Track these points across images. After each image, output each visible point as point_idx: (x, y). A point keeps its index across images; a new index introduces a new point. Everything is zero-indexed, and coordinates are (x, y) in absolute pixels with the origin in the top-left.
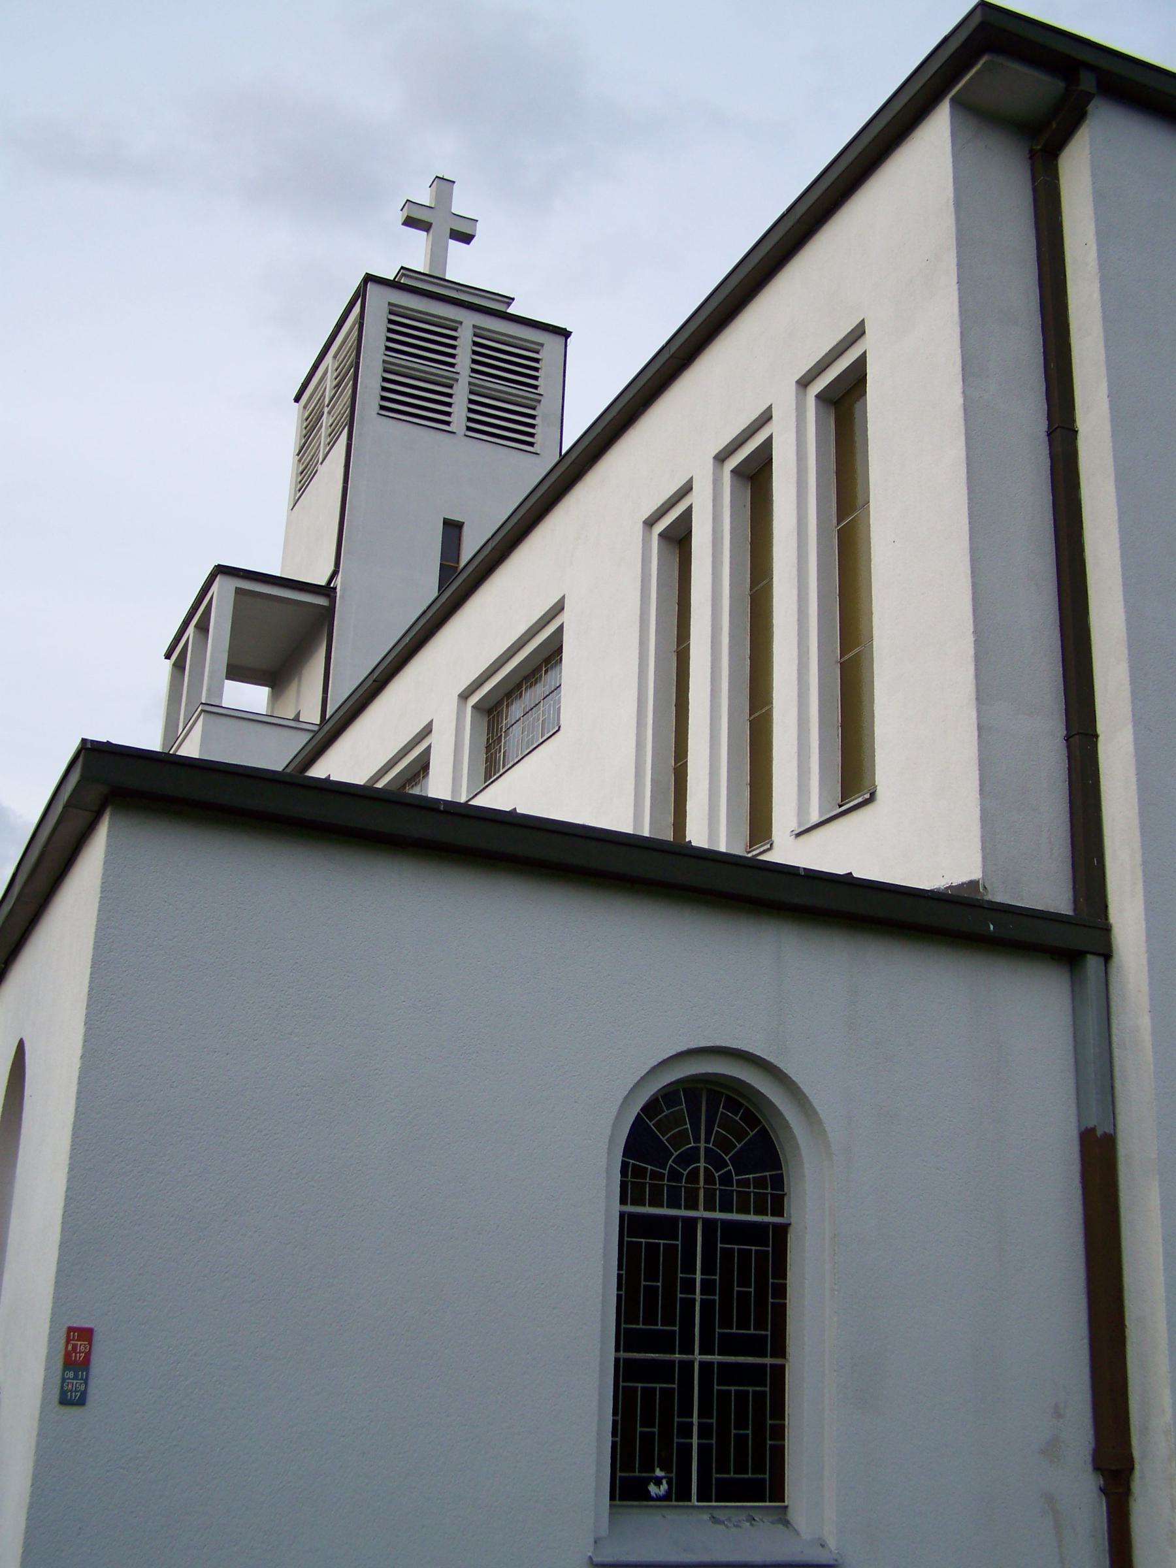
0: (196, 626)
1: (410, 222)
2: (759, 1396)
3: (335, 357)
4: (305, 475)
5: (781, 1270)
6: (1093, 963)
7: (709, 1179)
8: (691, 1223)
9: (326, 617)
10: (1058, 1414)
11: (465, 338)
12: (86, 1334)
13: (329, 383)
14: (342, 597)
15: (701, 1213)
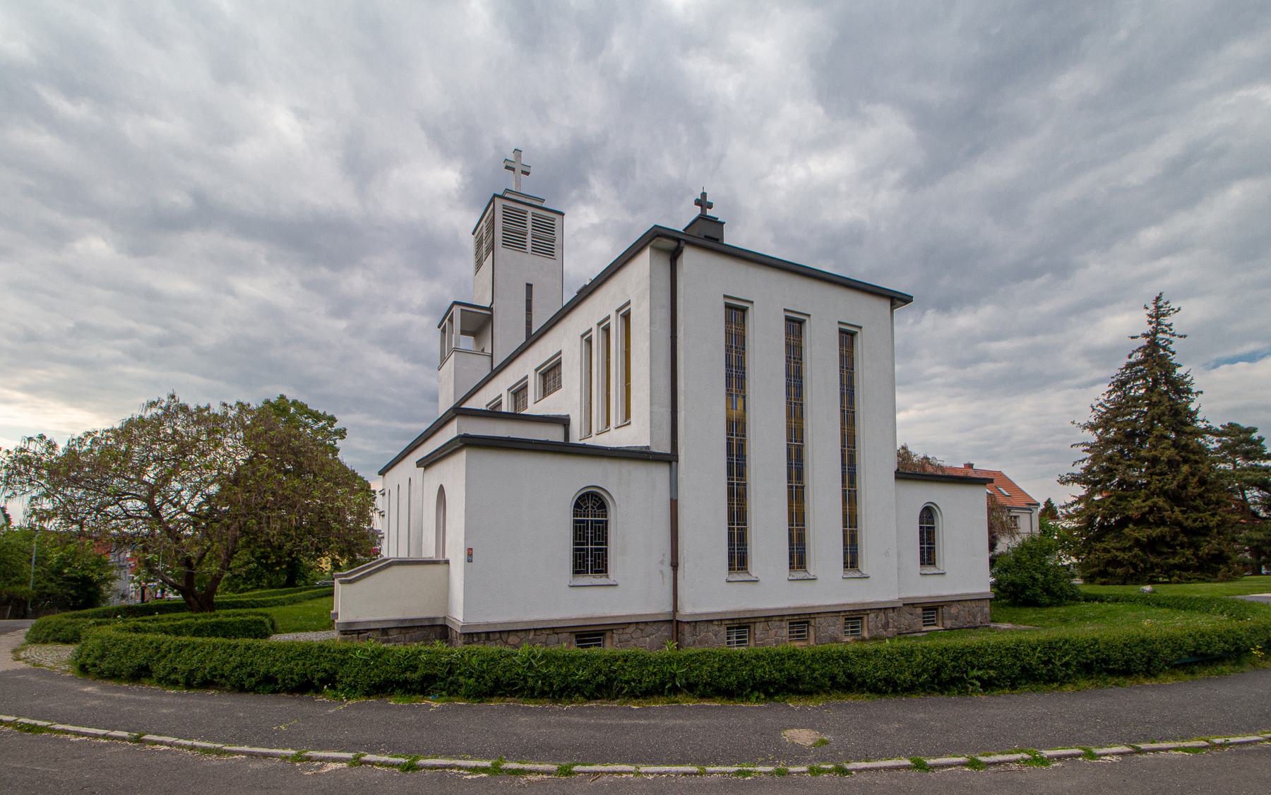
1: (507, 167)
2: (602, 554)
4: (479, 264)
5: (606, 529)
6: (674, 463)
7: (591, 511)
8: (588, 521)
9: (490, 318)
10: (664, 555)
11: (529, 217)
12: (471, 549)
13: (484, 229)
15: (590, 518)
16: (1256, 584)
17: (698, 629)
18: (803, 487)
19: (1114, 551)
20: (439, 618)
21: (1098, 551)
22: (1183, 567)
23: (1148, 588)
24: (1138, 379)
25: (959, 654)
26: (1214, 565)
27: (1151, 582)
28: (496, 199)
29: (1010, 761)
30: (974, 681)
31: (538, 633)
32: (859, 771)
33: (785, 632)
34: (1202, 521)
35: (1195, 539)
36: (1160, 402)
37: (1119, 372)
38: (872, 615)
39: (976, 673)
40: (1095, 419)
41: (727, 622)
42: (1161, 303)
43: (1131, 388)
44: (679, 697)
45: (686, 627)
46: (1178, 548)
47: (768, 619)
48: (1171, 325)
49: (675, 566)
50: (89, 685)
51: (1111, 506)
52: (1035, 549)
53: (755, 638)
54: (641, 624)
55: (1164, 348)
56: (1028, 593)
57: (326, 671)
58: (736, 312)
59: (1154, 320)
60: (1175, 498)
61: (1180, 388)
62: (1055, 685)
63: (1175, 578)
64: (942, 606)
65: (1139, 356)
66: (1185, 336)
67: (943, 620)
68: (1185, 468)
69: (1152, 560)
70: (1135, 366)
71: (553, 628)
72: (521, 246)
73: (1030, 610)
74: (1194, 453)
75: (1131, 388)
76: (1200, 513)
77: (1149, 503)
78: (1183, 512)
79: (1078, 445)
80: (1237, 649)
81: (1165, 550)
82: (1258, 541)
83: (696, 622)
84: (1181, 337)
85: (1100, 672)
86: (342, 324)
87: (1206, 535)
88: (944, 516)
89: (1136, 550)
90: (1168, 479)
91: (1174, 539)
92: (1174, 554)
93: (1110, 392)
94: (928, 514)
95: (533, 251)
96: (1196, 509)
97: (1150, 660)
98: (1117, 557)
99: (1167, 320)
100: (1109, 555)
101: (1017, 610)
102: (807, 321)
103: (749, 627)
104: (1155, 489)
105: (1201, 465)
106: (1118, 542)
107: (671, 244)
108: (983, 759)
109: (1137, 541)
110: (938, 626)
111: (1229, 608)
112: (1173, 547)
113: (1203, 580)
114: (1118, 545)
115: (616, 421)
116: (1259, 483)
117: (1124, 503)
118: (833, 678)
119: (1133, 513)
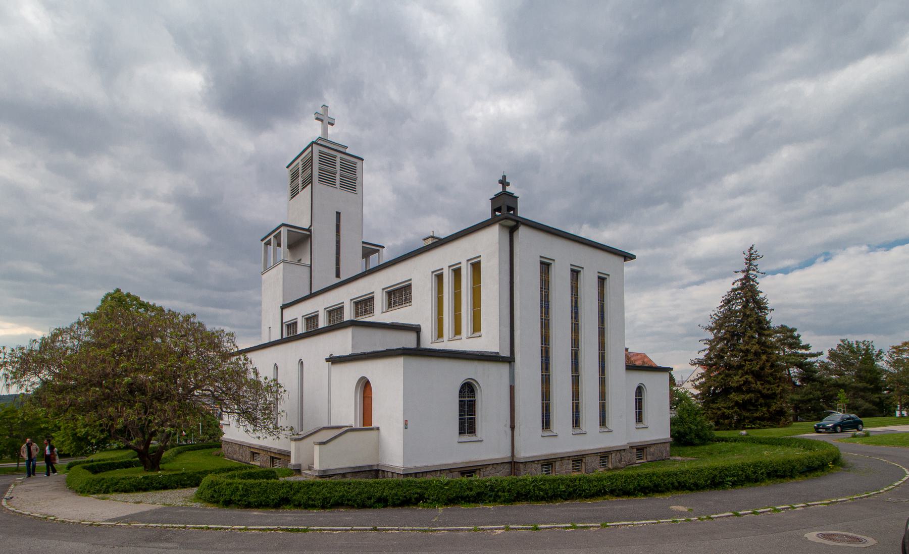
0: (274, 236)
1: (317, 119)
3: (302, 160)
6: (512, 363)
9: (310, 236)
11: (338, 160)
12: (407, 421)
14: (313, 233)
15: (466, 399)
16: (800, 428)
17: (527, 467)
18: (578, 376)
20: (374, 465)
22: (762, 419)
23: (744, 432)
25: (722, 470)
26: (778, 417)
27: (744, 428)
28: (314, 145)
29: (767, 511)
30: (728, 483)
31: (442, 472)
32: (716, 518)
33: (570, 466)
34: (772, 390)
35: (768, 401)
36: (751, 315)
37: (727, 294)
38: (614, 455)
39: (729, 479)
41: (542, 462)
42: (752, 251)
43: (733, 304)
44: (607, 497)
45: (521, 465)
46: (759, 406)
47: (562, 458)
48: (757, 265)
49: (513, 427)
50: (256, 512)
51: (722, 381)
52: (691, 410)
54: (495, 465)
56: (687, 438)
57: (418, 493)
58: (545, 266)
60: (758, 376)
61: (760, 306)
62: (758, 483)
66: (765, 273)
67: (646, 456)
68: (764, 357)
69: (744, 414)
71: (450, 469)
73: (689, 448)
74: (768, 347)
75: (733, 304)
76: (771, 384)
77: (743, 378)
78: (762, 384)
79: (703, 340)
81: (751, 408)
82: (797, 400)
83: (526, 462)
84: (762, 274)
85: (773, 477)
86: (87, 207)
87: (773, 398)
88: (647, 389)
89: (736, 408)
90: (754, 364)
91: (756, 401)
92: (757, 410)
93: (721, 307)
94: (640, 390)
95: (341, 187)
96: (769, 383)
97: (792, 470)
98: (724, 413)
99: (755, 262)
100: (720, 412)
101: (681, 448)
102: (582, 272)
103: (552, 464)
104: (747, 370)
105: (772, 355)
107: (512, 223)
108: (740, 513)
109: (737, 403)
111: (802, 444)
112: (756, 406)
113: (772, 427)
114: (725, 405)
115: (467, 334)
116: (798, 364)
117: (729, 379)
118: (672, 484)
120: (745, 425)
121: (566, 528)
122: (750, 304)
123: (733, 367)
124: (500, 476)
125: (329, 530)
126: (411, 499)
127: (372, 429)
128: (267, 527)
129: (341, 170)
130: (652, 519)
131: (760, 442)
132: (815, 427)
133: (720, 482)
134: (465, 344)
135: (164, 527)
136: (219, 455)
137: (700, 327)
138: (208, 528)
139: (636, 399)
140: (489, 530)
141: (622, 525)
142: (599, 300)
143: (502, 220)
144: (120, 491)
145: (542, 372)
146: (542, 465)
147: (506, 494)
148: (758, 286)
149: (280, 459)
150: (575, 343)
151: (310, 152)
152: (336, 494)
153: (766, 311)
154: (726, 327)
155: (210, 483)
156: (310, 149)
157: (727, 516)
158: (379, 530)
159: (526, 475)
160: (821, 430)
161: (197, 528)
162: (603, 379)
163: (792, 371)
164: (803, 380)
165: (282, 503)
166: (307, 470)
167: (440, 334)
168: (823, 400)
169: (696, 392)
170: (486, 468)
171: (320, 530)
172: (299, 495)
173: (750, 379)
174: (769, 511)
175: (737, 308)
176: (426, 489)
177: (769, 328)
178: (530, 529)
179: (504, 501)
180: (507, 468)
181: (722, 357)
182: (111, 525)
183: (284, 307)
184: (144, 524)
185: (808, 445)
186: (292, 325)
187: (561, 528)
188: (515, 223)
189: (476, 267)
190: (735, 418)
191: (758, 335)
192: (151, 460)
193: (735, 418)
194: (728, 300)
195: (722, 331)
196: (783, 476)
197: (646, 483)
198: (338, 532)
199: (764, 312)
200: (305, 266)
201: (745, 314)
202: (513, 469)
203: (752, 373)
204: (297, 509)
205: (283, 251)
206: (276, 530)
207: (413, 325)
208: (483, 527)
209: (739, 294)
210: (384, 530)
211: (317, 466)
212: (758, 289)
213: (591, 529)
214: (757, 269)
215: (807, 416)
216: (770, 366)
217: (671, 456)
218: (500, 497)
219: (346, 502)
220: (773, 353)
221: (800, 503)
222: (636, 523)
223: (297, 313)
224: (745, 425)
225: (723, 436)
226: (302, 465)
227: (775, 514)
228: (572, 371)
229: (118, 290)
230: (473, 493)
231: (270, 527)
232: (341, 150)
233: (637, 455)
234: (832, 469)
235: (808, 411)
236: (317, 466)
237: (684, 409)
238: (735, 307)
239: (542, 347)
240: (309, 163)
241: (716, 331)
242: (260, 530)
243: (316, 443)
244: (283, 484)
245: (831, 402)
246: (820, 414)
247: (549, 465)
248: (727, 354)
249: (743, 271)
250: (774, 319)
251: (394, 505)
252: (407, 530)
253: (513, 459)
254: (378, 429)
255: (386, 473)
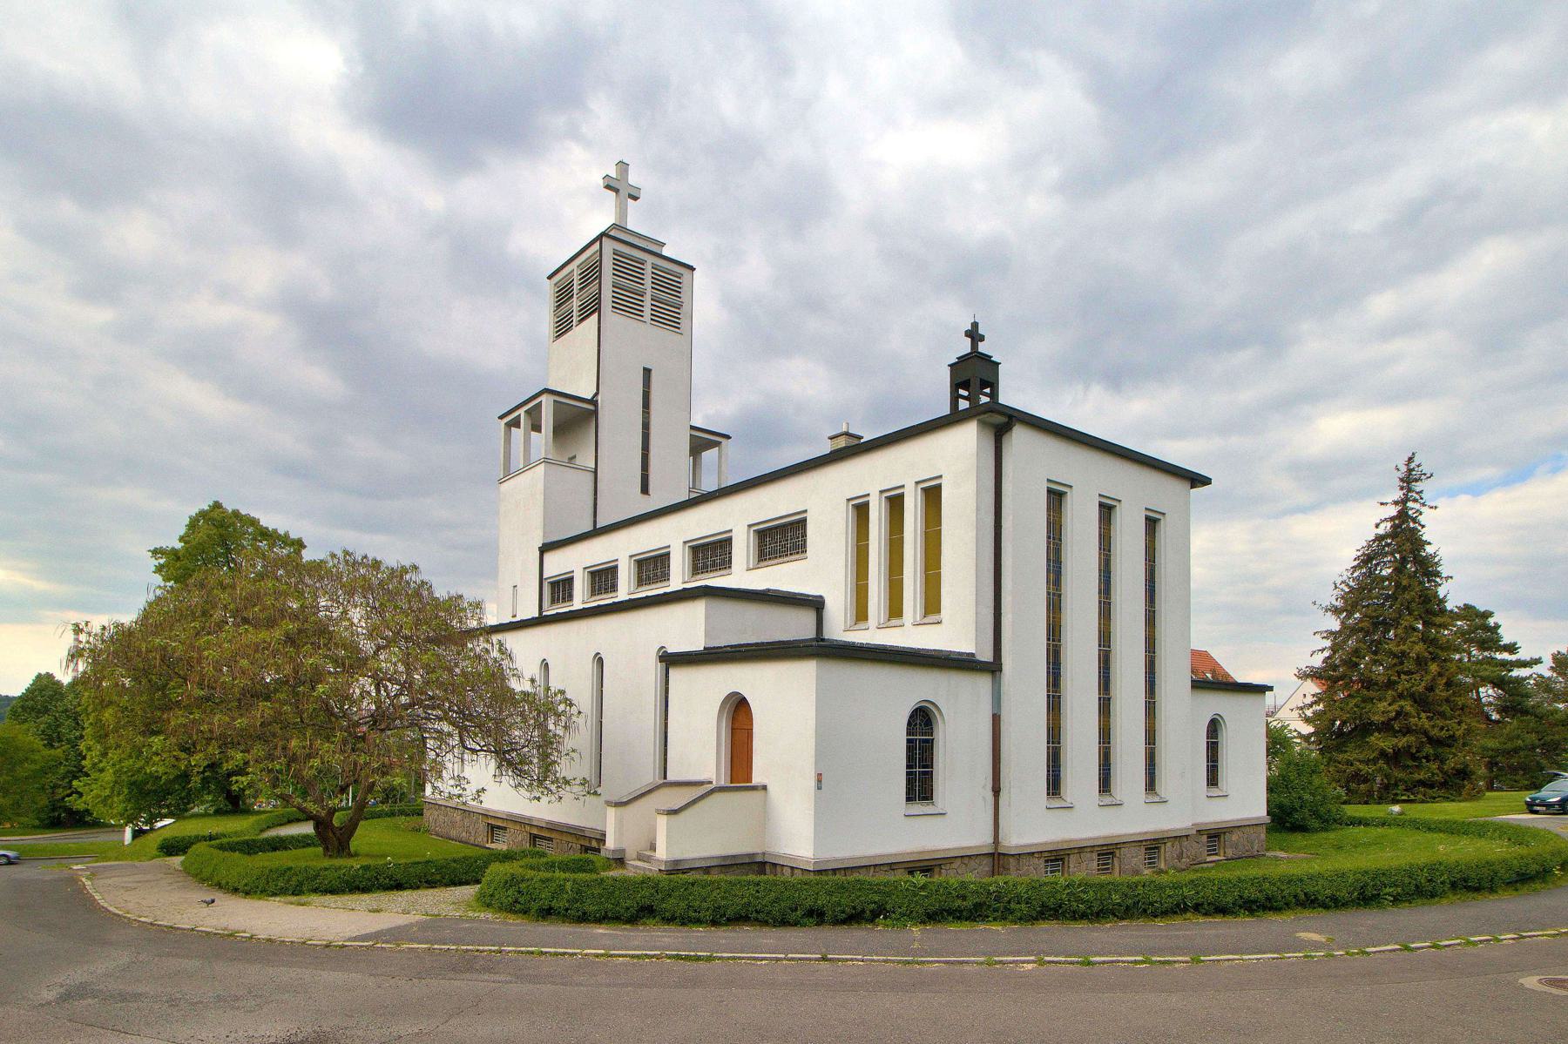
1: (608, 187)
3: (578, 267)
9: (596, 412)
11: (648, 269)
18: (1109, 699)
19: (1358, 763)
21: (1339, 763)
23: (1396, 808)
24: (1386, 554)
25: (1379, 875)
26: (1458, 781)
27: (1395, 802)
28: (604, 239)
31: (877, 868)
32: (1375, 952)
35: (1440, 750)
38: (1169, 844)
39: (1388, 890)
40: (1337, 599)
42: (1412, 465)
43: (1378, 564)
44: (1189, 915)
45: (1011, 860)
47: (1081, 850)
48: (1421, 492)
49: (996, 791)
53: (1069, 872)
54: (966, 858)
55: (1415, 520)
57: (875, 903)
59: (1405, 485)
61: (1428, 569)
63: (1420, 796)
64: (1225, 833)
65: (1385, 528)
68: (1434, 667)
70: (1383, 540)
72: (635, 311)
74: (1442, 649)
75: (1378, 564)
76: (1446, 719)
80: (1544, 870)
81: (1410, 763)
84: (1432, 508)
86: (102, 315)
87: (1450, 746)
90: (1415, 680)
93: (1355, 568)
94: (1214, 727)
96: (1442, 715)
97: (1493, 878)
99: (1418, 486)
100: (1352, 769)
101: (1284, 835)
102: (1118, 508)
106: (1360, 752)
107: (1000, 419)
109: (1383, 754)
110: (1220, 856)
113: (1447, 799)
114: (1361, 757)
116: (1495, 681)
119: (1377, 718)
120: (1396, 794)
121: (1136, 962)
122: (1409, 566)
123: (1376, 684)
124: (973, 876)
125: (749, 958)
126: (863, 911)
127: (754, 788)
128: (644, 952)
129: (652, 288)
130: (1271, 952)
131: (1429, 827)
132: (1527, 803)
133: (1373, 895)
134: (910, 635)
135: (463, 950)
136: (418, 830)
137: (1317, 606)
138: (542, 953)
139: (1207, 743)
140: (1011, 963)
141: (1226, 960)
142: (1146, 560)
143: (985, 413)
144: (321, 891)
145: (1048, 691)
146: (1047, 861)
147: (1023, 906)
148: (1423, 530)
149: (551, 839)
150: (1105, 638)
151: (597, 252)
152: (737, 900)
153: (1438, 580)
154: (1364, 607)
155: (508, 877)
156: (597, 246)
157: (1391, 951)
158: (830, 960)
159: (1017, 878)
160: (1538, 808)
161: (522, 952)
162: (1152, 705)
163: (1485, 694)
164: (1503, 710)
165: (641, 914)
166: (634, 860)
167: (861, 614)
168: (1542, 749)
169: (1307, 729)
170: (950, 863)
171: (734, 958)
172: (672, 901)
173: (1408, 708)
174: (1458, 944)
175: (1384, 573)
176: (889, 895)
177: (1443, 611)
178: (1078, 963)
179: (1021, 919)
180: (986, 865)
181: (1356, 665)
182: (366, 946)
183: (545, 549)
184: (426, 946)
185: (1516, 835)
186: (561, 587)
187: (1128, 962)
188: (1007, 420)
189: (932, 495)
190: (1378, 779)
191: (1423, 625)
192: (333, 838)
193: (1378, 779)
194: (1368, 555)
195: (1355, 616)
196: (1477, 889)
197: (1252, 893)
198: (763, 962)
199: (1435, 581)
200: (585, 470)
201: (1398, 585)
202: (996, 867)
203: (1412, 696)
204: (668, 925)
205: (542, 441)
206: (658, 957)
207: (809, 596)
208: (1001, 959)
209: (1388, 545)
210: (839, 960)
211: (662, 853)
212: (1424, 538)
213: (1177, 965)
214: (1421, 498)
215: (1511, 779)
216: (1446, 683)
217: (1268, 850)
218: (1012, 912)
219: (754, 915)
220: (1451, 660)
221: (1510, 932)
222: (1247, 957)
223: (575, 562)
224: (1396, 794)
225: (1357, 815)
226: (627, 851)
227: (1470, 949)
228: (1099, 690)
229: (217, 505)
230: (968, 904)
231: (648, 952)
232: (652, 249)
233: (1208, 847)
234: (1560, 878)
235: (1514, 770)
236: (662, 853)
237: (1289, 763)
238: (1381, 570)
239: (1048, 645)
240: (592, 273)
241: (1345, 614)
242: (633, 956)
243: (659, 812)
244: (643, 882)
245: (1557, 755)
246: (1536, 778)
247: (1057, 860)
248: (1364, 658)
249: (1396, 503)
250: (1454, 594)
251: (837, 922)
252: (878, 961)
253: (996, 849)
254: (765, 788)
255: (779, 868)
